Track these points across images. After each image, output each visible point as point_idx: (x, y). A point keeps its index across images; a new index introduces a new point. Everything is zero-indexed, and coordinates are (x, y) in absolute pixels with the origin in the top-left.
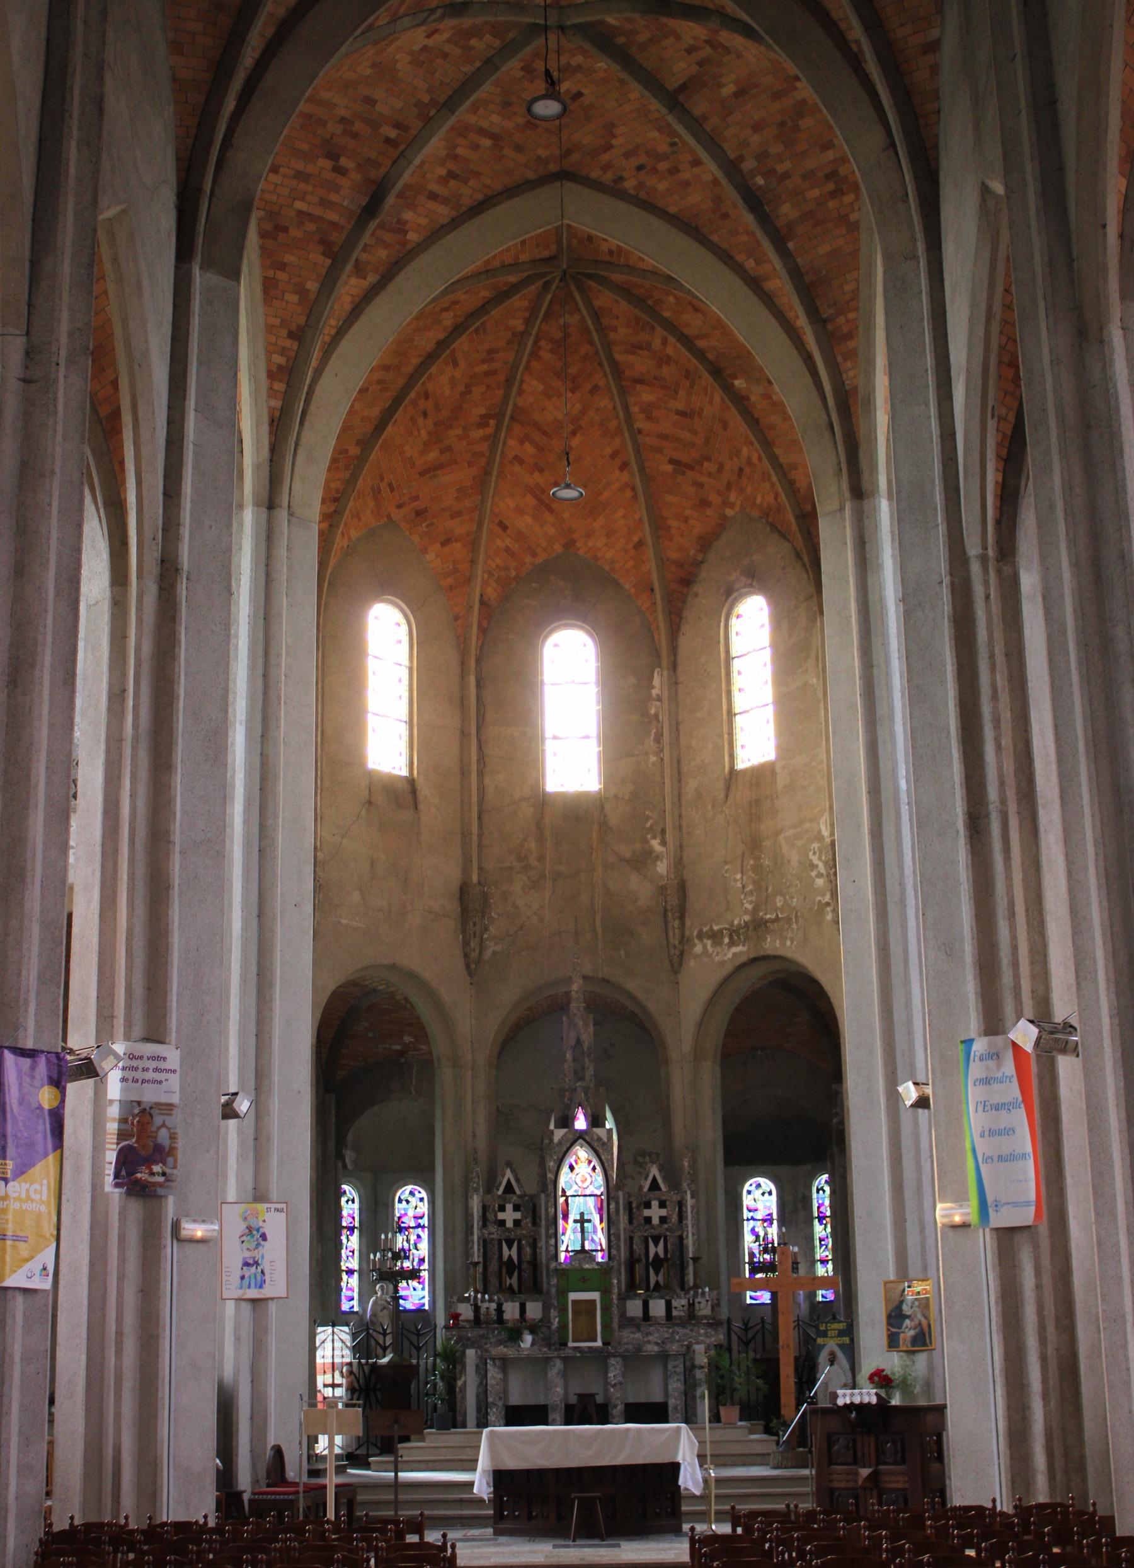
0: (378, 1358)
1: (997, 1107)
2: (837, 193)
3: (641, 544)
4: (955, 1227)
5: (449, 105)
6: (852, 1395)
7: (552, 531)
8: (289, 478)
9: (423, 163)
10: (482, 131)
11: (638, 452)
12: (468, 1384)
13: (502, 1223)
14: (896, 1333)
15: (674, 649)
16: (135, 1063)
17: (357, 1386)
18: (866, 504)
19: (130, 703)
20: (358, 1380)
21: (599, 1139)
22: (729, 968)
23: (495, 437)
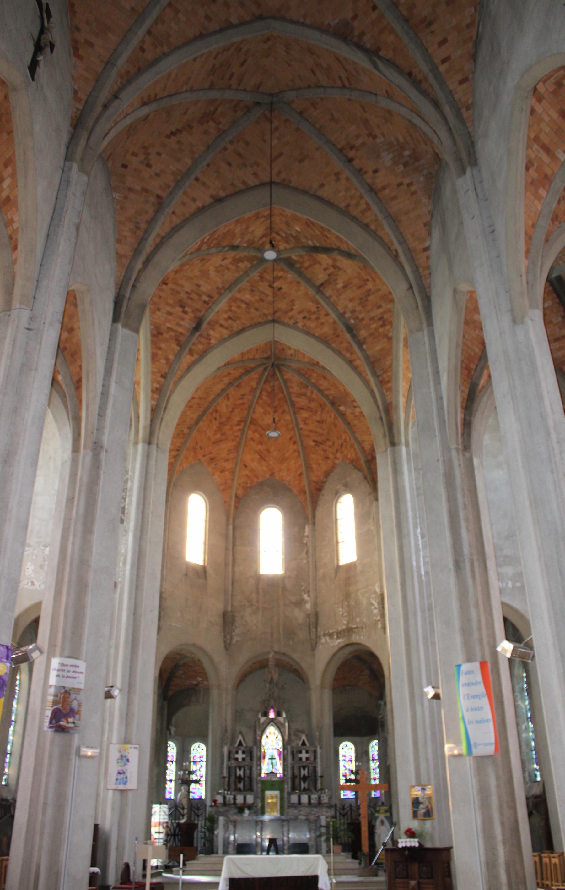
0: (179, 819)
1: (474, 697)
2: (383, 325)
3: (301, 474)
4: (454, 756)
6: (406, 842)
7: (265, 469)
9: (218, 312)
10: (242, 301)
11: (300, 436)
13: (237, 759)
14: (416, 811)
15: (314, 517)
16: (64, 668)
17: (169, 833)
18: (396, 448)
19: (76, 503)
20: (170, 830)
21: (280, 722)
22: (336, 649)
23: (243, 429)
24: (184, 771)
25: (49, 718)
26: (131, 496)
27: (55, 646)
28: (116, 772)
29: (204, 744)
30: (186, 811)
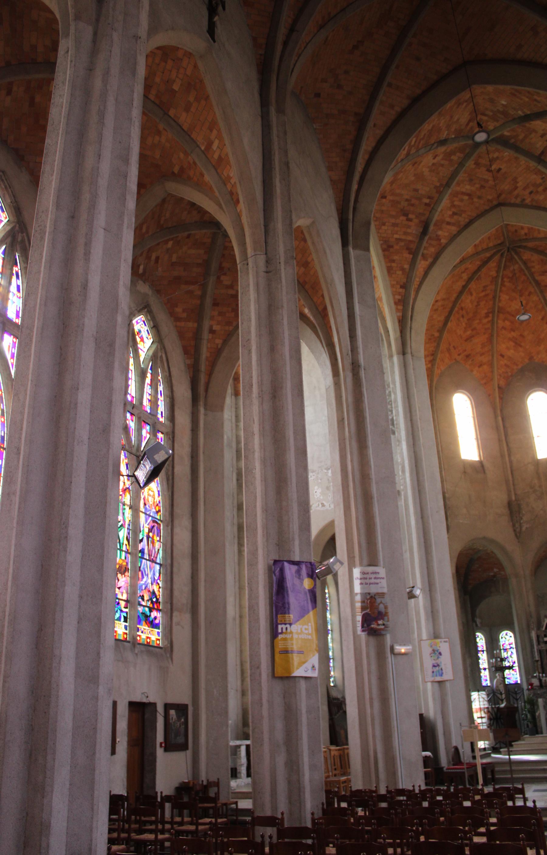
0: (499, 704)
5: (448, 185)
8: (409, 342)
9: (442, 210)
10: (463, 193)
12: (541, 714)
16: (365, 576)
17: (492, 717)
19: (346, 423)
20: (492, 715)
23: (493, 320)
24: (496, 658)
25: (360, 622)
26: (397, 407)
27: (354, 557)
28: (431, 666)
29: (511, 631)
30: (504, 696)
